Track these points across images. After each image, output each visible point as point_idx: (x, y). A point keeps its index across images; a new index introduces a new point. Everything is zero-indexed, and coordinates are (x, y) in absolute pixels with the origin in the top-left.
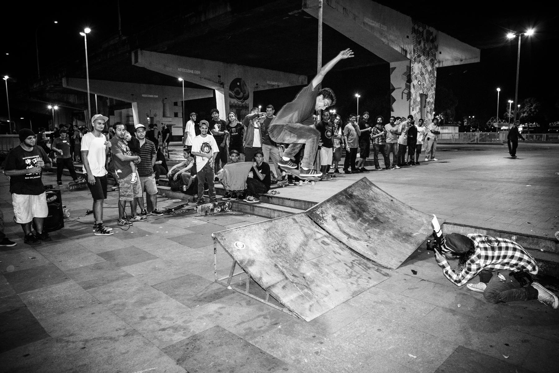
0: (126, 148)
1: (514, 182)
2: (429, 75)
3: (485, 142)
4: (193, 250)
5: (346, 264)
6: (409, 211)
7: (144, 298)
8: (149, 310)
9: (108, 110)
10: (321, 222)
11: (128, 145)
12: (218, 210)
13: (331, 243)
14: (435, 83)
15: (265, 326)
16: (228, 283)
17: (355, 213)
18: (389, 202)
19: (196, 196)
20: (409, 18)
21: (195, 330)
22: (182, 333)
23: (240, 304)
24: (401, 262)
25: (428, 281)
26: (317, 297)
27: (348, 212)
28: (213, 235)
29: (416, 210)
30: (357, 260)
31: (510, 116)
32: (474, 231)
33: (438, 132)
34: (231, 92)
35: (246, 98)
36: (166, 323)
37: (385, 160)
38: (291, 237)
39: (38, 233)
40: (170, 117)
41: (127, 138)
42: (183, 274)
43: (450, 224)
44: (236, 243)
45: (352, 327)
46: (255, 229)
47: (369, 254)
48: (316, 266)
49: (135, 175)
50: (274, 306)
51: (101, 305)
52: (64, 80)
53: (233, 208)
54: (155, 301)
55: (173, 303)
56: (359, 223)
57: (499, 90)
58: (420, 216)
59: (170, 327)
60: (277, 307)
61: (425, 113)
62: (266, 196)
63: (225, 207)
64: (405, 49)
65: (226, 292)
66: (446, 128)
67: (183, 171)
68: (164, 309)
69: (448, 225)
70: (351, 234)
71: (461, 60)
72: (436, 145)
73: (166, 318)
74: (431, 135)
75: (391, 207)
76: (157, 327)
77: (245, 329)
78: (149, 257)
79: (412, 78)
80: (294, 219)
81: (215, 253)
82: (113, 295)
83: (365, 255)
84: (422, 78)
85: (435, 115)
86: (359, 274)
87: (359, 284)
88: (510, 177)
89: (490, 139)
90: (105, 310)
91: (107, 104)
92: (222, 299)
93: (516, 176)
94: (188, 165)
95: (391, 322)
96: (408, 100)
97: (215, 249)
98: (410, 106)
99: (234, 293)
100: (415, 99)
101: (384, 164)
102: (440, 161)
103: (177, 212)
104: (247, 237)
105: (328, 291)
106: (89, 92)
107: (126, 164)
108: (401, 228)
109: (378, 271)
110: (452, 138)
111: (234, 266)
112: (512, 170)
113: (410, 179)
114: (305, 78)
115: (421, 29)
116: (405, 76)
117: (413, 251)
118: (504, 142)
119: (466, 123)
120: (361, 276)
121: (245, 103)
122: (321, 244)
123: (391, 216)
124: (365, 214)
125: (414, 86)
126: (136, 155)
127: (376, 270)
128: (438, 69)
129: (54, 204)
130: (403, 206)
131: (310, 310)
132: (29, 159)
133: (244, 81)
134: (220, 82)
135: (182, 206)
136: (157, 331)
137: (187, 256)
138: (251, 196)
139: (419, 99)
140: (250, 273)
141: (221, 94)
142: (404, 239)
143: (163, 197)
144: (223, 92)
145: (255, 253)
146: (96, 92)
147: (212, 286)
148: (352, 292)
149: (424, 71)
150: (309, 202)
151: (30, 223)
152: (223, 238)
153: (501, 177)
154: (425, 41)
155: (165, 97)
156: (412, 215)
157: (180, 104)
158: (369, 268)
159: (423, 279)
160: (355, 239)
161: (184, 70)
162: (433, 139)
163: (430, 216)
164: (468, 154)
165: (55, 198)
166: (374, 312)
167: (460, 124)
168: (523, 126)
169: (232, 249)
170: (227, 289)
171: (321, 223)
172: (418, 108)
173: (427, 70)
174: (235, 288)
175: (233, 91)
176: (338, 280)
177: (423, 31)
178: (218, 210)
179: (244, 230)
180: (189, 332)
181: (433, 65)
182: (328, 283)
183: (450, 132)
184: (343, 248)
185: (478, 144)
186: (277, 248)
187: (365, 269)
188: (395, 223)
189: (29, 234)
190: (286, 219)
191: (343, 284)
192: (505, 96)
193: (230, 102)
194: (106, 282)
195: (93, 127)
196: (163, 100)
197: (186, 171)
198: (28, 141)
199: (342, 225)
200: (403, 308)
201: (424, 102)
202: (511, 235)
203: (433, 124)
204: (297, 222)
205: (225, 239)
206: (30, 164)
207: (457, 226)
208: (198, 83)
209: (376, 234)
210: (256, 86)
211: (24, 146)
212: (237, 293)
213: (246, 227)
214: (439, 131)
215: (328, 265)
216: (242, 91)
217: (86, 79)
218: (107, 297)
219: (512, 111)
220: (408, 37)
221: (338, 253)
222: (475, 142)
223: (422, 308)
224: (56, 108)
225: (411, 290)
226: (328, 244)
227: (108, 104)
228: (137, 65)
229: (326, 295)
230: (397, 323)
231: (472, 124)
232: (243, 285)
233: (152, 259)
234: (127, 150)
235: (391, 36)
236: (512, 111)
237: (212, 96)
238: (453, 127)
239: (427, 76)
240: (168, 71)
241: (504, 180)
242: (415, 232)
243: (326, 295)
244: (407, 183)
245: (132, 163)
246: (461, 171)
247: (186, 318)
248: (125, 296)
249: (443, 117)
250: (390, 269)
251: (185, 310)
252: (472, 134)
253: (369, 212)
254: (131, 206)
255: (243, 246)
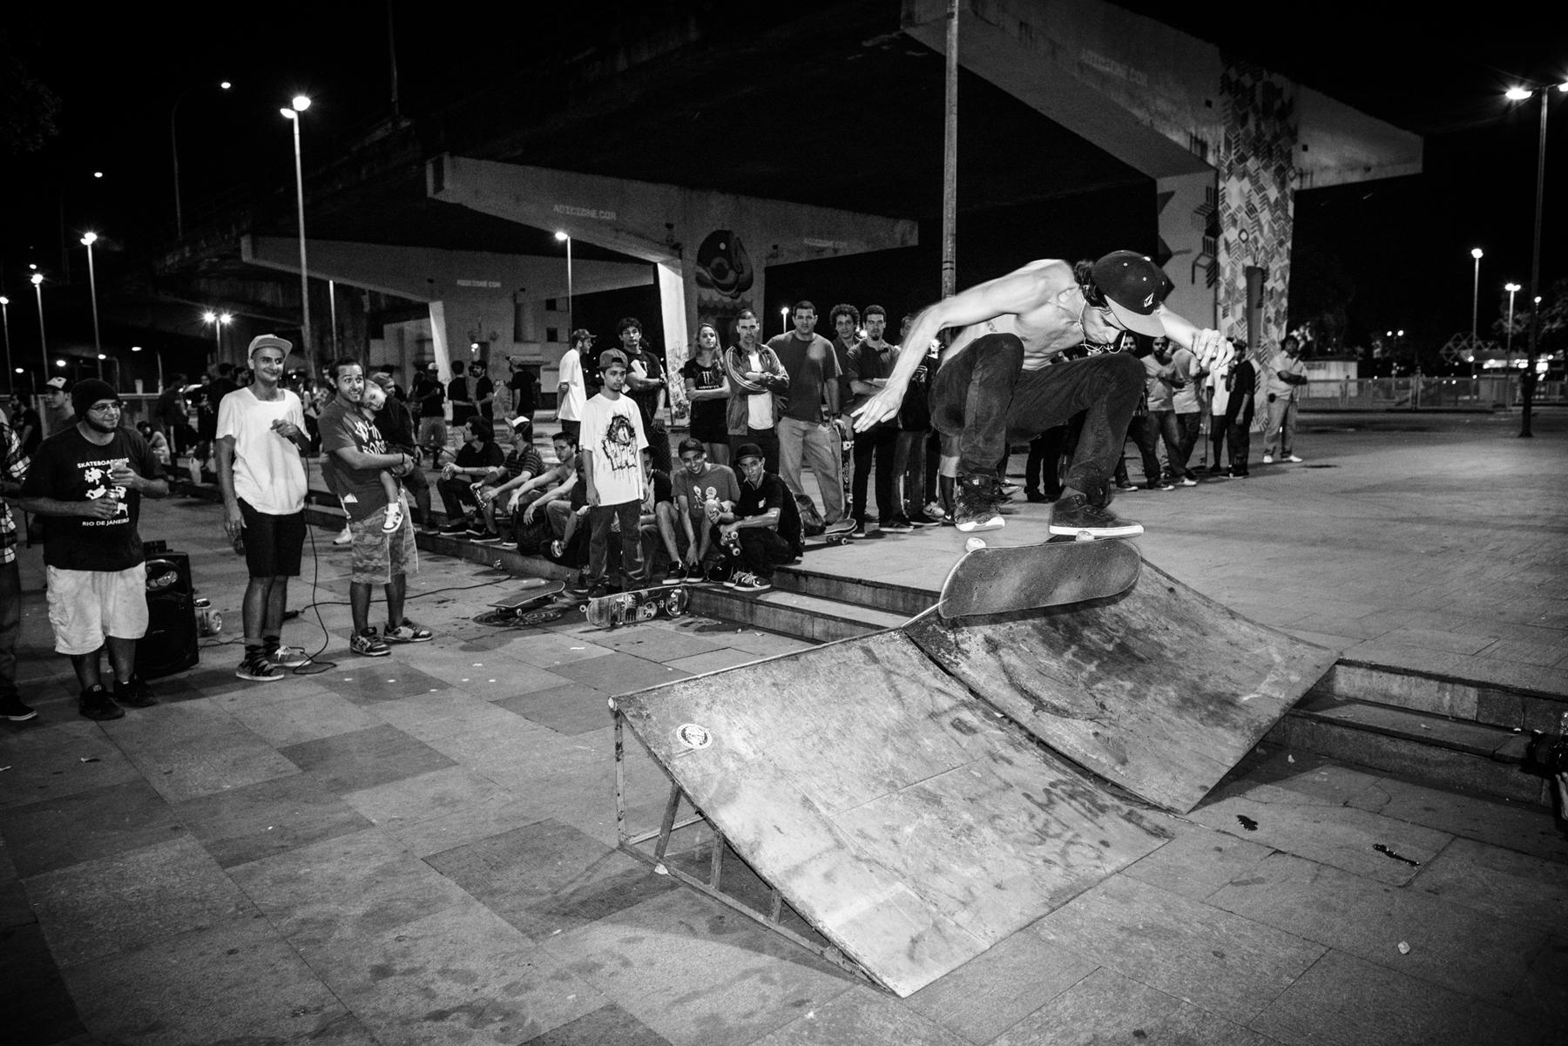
0: (370, 432)
1: (1542, 528)
2: (1272, 213)
3: (1440, 405)
4: (562, 739)
5: (1028, 797)
6: (1225, 624)
7: (396, 900)
8: (404, 944)
9: (364, 323)
10: (952, 658)
11: (376, 423)
12: (649, 611)
13: (983, 726)
14: (1290, 235)
15: (764, 1011)
16: (657, 854)
17: (1058, 629)
18: (1164, 595)
19: (586, 571)
20: (1211, 50)
21: (539, 1021)
22: (497, 1031)
23: (692, 929)
24: (1204, 788)
25: (1293, 855)
26: (934, 909)
27: (1034, 626)
28: (611, 703)
29: (1247, 620)
30: (1065, 783)
31: (1510, 330)
32: (1436, 688)
33: (1300, 377)
34: (701, 270)
35: (747, 285)
36: (450, 992)
37: (1144, 461)
38: (858, 707)
39: (117, 683)
40: (534, 342)
41: (373, 401)
42: (525, 818)
43: (1358, 665)
44: (684, 730)
45: (1048, 1023)
46: (744, 683)
47: (1102, 762)
48: (935, 802)
49: (397, 510)
50: (797, 937)
51: (260, 925)
52: (245, 243)
53: (692, 608)
54: (426, 912)
55: (483, 917)
56: (1070, 662)
57: (1477, 253)
58: (1260, 640)
59: (459, 1009)
60: (806, 943)
61: (1259, 320)
62: (789, 571)
63: (669, 603)
64: (1199, 137)
65: (653, 885)
66: (1320, 366)
67: (552, 497)
68: (451, 942)
69: (1352, 670)
70: (1045, 696)
71: (1368, 169)
72: (1295, 416)
73: (455, 972)
74: (1281, 388)
75: (1168, 610)
76: (422, 1006)
77: (700, 1021)
78: (431, 759)
79: (1223, 223)
80: (867, 651)
81: (618, 760)
82: (303, 888)
83: (1088, 764)
84: (1250, 221)
85: (1289, 329)
86: (1073, 829)
87: (1069, 866)
88: (1528, 512)
89: (1453, 398)
90: (271, 940)
91: (363, 306)
92: (636, 910)
93: (1548, 509)
94: (568, 477)
95: (1177, 1005)
96: (1209, 286)
97: (619, 746)
98: (1216, 304)
99: (673, 886)
100: (1231, 283)
101: (1141, 472)
102: (1309, 463)
103: (528, 617)
104: (719, 707)
105: (973, 889)
106: (304, 273)
107: (367, 478)
108: (1201, 677)
109: (1130, 821)
110: (1338, 394)
111: (674, 804)
112: (1531, 491)
113: (1219, 518)
114: (913, 228)
115: (1247, 81)
116: (1201, 217)
117: (1241, 754)
118: (1494, 406)
119: (1378, 350)
120: (1077, 835)
121: (743, 300)
122: (950, 729)
123: (1171, 637)
124: (1089, 634)
125: (1227, 244)
126: (397, 452)
127: (1124, 818)
128: (1299, 196)
129: (169, 597)
130: (1204, 608)
131: (911, 957)
132: (96, 467)
133: (738, 239)
134: (672, 241)
135: (547, 600)
136: (418, 1020)
137: (544, 758)
138: (748, 572)
139: (1242, 283)
140: (721, 827)
141: (673, 274)
142: (1212, 714)
143: (495, 572)
144: (681, 272)
145: (740, 759)
146: (331, 274)
147: (608, 862)
148: (1048, 890)
149: (1256, 200)
150: (917, 592)
151: (97, 654)
152: (644, 713)
153: (1503, 513)
154: (1261, 115)
155: (522, 286)
156: (1235, 638)
157: (560, 305)
158: (1103, 809)
159: (1276, 847)
160: (1058, 711)
161: (570, 210)
162: (1287, 398)
163: (1291, 638)
164: (1390, 443)
165: (171, 577)
166: (1121, 965)
167: (1361, 355)
168: (1551, 357)
169: (670, 748)
170: (653, 872)
171: (952, 662)
172: (1239, 309)
173: (1265, 199)
174: (679, 873)
175: (709, 265)
176: (1005, 849)
177: (1254, 85)
178: (649, 611)
179: (711, 685)
180: (520, 1025)
181: (1282, 185)
182: (971, 860)
183: (1333, 376)
184: (1020, 744)
185: (1417, 411)
186: (810, 744)
187: (1090, 811)
188: (1180, 662)
189: (91, 688)
190: (842, 651)
191: (1019, 863)
192: (1495, 272)
193: (700, 299)
194: (288, 843)
195: (252, 373)
196: (515, 295)
197: (561, 497)
198: (96, 415)
199: (1015, 667)
200: (1215, 954)
201: (1256, 291)
202: (1559, 706)
203: (1285, 353)
204: (875, 660)
205: (648, 716)
206: (98, 482)
207: (1382, 674)
208: (609, 247)
209: (1125, 697)
210: (771, 250)
211: (86, 431)
212: (681, 889)
213: (717, 678)
214: (1303, 374)
215: (972, 800)
216: (732, 267)
217: (298, 236)
218: (285, 894)
219: (1518, 316)
220: (1209, 104)
221: (1003, 758)
222: (1408, 405)
223: (1281, 954)
224: (227, 319)
225: (1240, 889)
226: (972, 730)
227: (367, 309)
228: (441, 197)
229: (963, 903)
230: (1198, 1010)
231: (1398, 353)
232: (706, 859)
233: (436, 769)
234: (372, 439)
235: (1159, 102)
236: (1518, 316)
237: (651, 282)
238: (1340, 364)
239: (1265, 216)
240: (527, 214)
241: (1513, 523)
242: (1246, 692)
243: (963, 903)
244: (1213, 533)
245: (385, 475)
246: (1377, 495)
247: (515, 974)
248: (340, 890)
249: (1311, 335)
250: (1169, 810)
251: (516, 946)
252: (1397, 383)
253: (1100, 626)
254: (389, 599)
255: (706, 738)
